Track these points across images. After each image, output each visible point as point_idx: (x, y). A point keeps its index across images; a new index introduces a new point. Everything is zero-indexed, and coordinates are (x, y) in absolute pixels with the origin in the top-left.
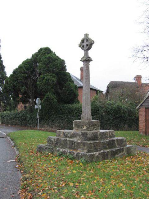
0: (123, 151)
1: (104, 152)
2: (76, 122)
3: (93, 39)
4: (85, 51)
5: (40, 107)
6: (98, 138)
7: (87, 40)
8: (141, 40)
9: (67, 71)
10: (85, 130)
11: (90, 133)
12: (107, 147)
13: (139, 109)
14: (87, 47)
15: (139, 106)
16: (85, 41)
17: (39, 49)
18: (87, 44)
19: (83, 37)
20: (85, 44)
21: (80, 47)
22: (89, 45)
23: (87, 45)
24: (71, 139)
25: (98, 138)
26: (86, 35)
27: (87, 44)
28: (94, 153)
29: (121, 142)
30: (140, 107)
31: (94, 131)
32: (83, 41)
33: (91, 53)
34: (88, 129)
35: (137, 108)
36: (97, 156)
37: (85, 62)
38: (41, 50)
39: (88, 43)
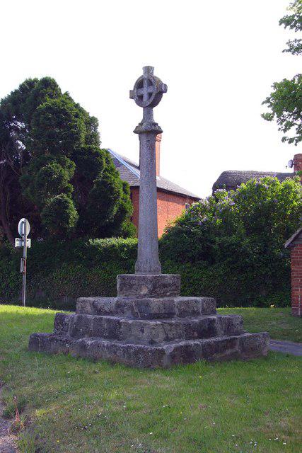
0: (232, 346)
1: (187, 346)
2: (123, 278)
3: (164, 82)
4: (144, 108)
5: (28, 243)
6: (174, 314)
7: (150, 83)
8: (290, 68)
9: (102, 147)
10: (145, 295)
11: (156, 302)
12: (196, 334)
13: (290, 247)
14: (151, 100)
15: (290, 240)
16: (145, 84)
17: (22, 81)
18: (148, 91)
19: (140, 73)
20: (145, 91)
21: (131, 98)
22: (154, 95)
23: (150, 95)
24: (111, 318)
25: (174, 314)
26: (148, 70)
27: (148, 91)
28: (164, 348)
29: (229, 326)
30: (296, 243)
31: (166, 299)
32: (139, 84)
33: (159, 114)
34: (152, 293)
35: (286, 246)
36: (171, 353)
37: (144, 136)
38: (28, 86)
39: (151, 90)
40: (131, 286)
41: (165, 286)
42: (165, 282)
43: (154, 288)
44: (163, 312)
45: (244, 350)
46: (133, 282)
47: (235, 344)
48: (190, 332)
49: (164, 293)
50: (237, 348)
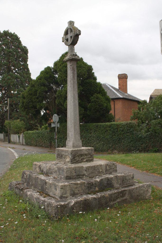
4: (69, 46)
16: (69, 32)
19: (66, 26)
26: (71, 23)
32: (66, 33)
40: (62, 156)
41: (82, 155)
42: (82, 153)
43: (74, 158)
44: (74, 174)
45: (132, 197)
46: (63, 153)
47: (125, 194)
48: (90, 188)
49: (81, 160)
50: (127, 197)
